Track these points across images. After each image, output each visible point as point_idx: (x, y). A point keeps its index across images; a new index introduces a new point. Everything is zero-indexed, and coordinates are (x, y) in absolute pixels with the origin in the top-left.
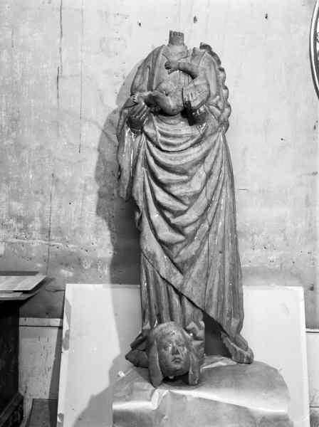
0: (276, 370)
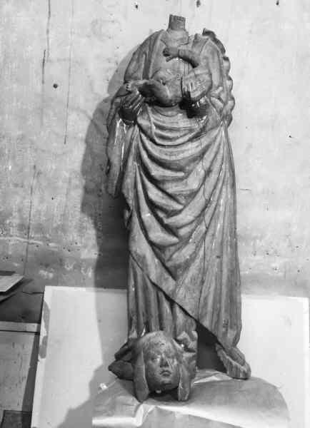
0: (275, 388)
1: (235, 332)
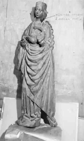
0: (61, 130)
1: (53, 112)
